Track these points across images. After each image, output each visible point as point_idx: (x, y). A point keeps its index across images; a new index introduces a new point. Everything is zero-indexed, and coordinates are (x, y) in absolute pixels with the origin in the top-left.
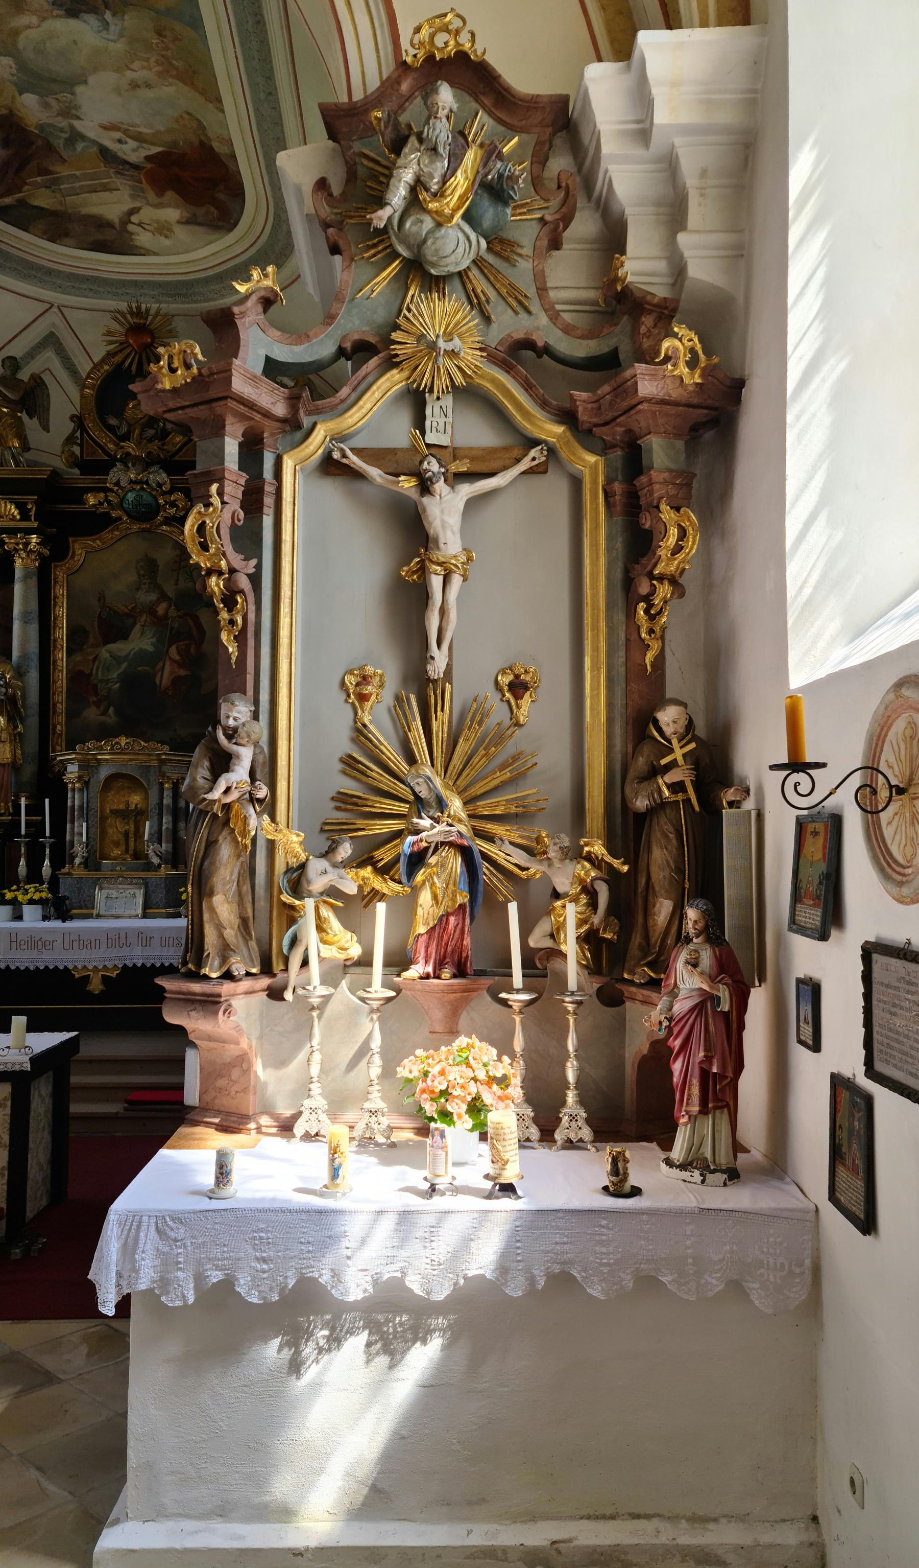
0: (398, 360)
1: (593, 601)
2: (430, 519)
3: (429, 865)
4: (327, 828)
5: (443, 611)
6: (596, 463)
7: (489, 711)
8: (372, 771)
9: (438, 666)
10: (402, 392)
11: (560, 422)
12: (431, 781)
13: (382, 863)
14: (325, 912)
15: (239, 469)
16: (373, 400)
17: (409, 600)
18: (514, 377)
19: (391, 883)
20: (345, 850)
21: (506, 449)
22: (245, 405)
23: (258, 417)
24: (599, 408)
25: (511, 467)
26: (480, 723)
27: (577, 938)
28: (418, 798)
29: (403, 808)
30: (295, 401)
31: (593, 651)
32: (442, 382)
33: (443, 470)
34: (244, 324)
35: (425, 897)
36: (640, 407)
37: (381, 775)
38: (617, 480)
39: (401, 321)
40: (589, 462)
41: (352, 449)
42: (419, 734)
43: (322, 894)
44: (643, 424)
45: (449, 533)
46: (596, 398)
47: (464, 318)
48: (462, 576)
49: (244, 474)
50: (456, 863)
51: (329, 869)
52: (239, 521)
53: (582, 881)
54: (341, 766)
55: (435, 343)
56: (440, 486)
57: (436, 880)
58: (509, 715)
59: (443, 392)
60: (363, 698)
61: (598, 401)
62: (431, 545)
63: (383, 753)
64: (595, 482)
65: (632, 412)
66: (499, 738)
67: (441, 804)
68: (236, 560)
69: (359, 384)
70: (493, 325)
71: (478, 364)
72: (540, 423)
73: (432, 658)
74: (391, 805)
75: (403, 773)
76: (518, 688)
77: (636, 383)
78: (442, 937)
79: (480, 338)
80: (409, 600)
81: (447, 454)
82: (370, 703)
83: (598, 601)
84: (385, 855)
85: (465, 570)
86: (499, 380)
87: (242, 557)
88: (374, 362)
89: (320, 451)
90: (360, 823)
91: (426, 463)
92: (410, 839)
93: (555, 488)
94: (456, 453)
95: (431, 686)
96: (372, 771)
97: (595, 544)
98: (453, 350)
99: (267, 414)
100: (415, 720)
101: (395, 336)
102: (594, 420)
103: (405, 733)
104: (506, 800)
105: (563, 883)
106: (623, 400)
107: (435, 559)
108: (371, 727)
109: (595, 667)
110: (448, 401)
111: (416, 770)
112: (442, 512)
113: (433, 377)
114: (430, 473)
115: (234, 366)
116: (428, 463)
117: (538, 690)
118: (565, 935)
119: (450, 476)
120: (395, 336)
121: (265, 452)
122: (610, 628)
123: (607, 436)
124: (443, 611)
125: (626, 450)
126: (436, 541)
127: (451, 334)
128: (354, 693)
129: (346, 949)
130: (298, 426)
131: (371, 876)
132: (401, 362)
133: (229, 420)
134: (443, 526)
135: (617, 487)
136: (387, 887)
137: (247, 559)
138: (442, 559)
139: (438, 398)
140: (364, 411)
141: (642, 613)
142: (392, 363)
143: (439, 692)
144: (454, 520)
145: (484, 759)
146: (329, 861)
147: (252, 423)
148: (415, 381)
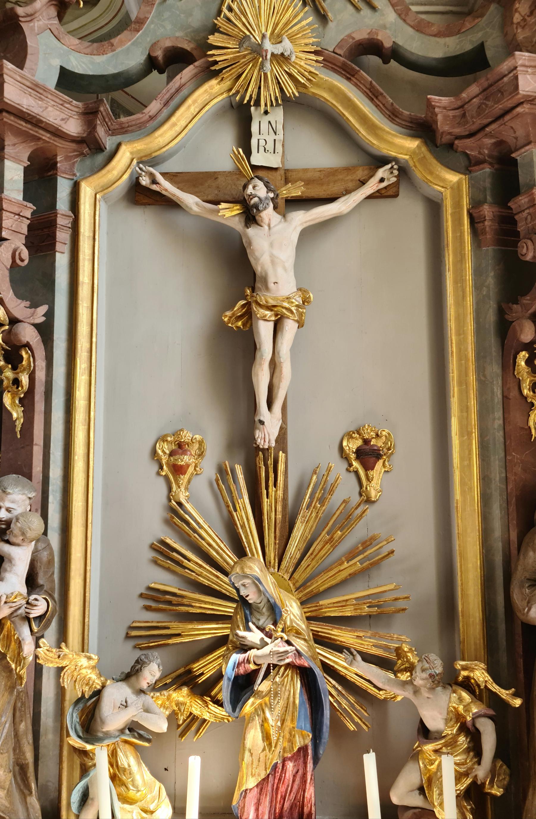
0: (217, 67)
1: (459, 350)
2: (257, 254)
3: (259, 694)
4: (134, 633)
5: (274, 365)
6: (459, 183)
7: (333, 486)
8: (189, 560)
9: (267, 434)
10: (224, 107)
11: (414, 136)
12: (260, 583)
13: (204, 678)
14: (128, 759)
15: (24, 199)
16: (189, 116)
17: (234, 350)
18: (356, 85)
19: (213, 707)
20: (152, 673)
21: (347, 170)
22: (27, 121)
23: (46, 136)
24: (464, 115)
25: (354, 190)
26: (322, 501)
27: (458, 796)
28: (243, 602)
29: (228, 608)
30: (91, 117)
31: (461, 410)
32: (270, 92)
33: (271, 195)
34: (32, 29)
35: (254, 737)
36: (519, 110)
37: (201, 566)
38: (485, 201)
39: (220, 22)
40: (449, 182)
41: (163, 174)
42: (246, 513)
43: (122, 731)
44: (520, 133)
45: (280, 271)
46: (459, 103)
47: (295, 16)
48: (297, 321)
49: (30, 205)
50: (295, 687)
51: (132, 698)
52: (22, 260)
53: (458, 717)
54: (152, 554)
55: (260, 46)
56: (268, 214)
57: (268, 714)
58: (357, 489)
59: (272, 105)
60: (178, 470)
61: (462, 107)
62: (258, 285)
63: (203, 539)
64: (457, 205)
65: (507, 118)
66: (347, 520)
67: (275, 611)
68: (19, 308)
69: (171, 98)
70: (330, 24)
71: (313, 70)
72: (389, 138)
73: (262, 423)
74: (212, 604)
75: (228, 563)
76: (368, 455)
77: (516, 78)
78: (278, 788)
79: (314, 40)
80: (234, 350)
81: (278, 176)
82: (187, 476)
83: (466, 350)
84: (206, 668)
85: (301, 314)
86: (339, 89)
87: (28, 303)
88: (189, 72)
89: (126, 176)
90: (176, 627)
91: (250, 187)
92: (236, 657)
93: (409, 212)
94: (288, 176)
95: (260, 453)
96: (189, 560)
97: (459, 280)
98: (282, 54)
99: (57, 133)
100: (241, 497)
101: (213, 39)
102: (457, 131)
103: (230, 512)
104: (356, 599)
105: (435, 720)
106: (498, 102)
107: (263, 302)
108: (188, 506)
109: (465, 431)
110: (278, 115)
111: (242, 569)
112: (271, 245)
113: (260, 88)
114: (256, 200)
115: (5, 70)
116: (254, 187)
117: (392, 458)
118: (441, 794)
119: (281, 203)
120: (213, 39)
121: (59, 179)
122: (483, 384)
123: (472, 150)
124: (274, 365)
125: (496, 166)
126: (265, 280)
127: (280, 36)
128: (168, 464)
129: (152, 812)
130: (99, 148)
131: (187, 700)
132: (221, 70)
133: (9, 140)
134: (273, 262)
135: (488, 211)
136: (209, 712)
137: (34, 305)
138: (272, 302)
139: (266, 113)
140: (178, 129)
141: (523, 363)
142: (210, 72)
143: (270, 462)
144: (287, 255)
145: (328, 546)
146: (131, 686)
147: (40, 144)
148: (238, 92)
